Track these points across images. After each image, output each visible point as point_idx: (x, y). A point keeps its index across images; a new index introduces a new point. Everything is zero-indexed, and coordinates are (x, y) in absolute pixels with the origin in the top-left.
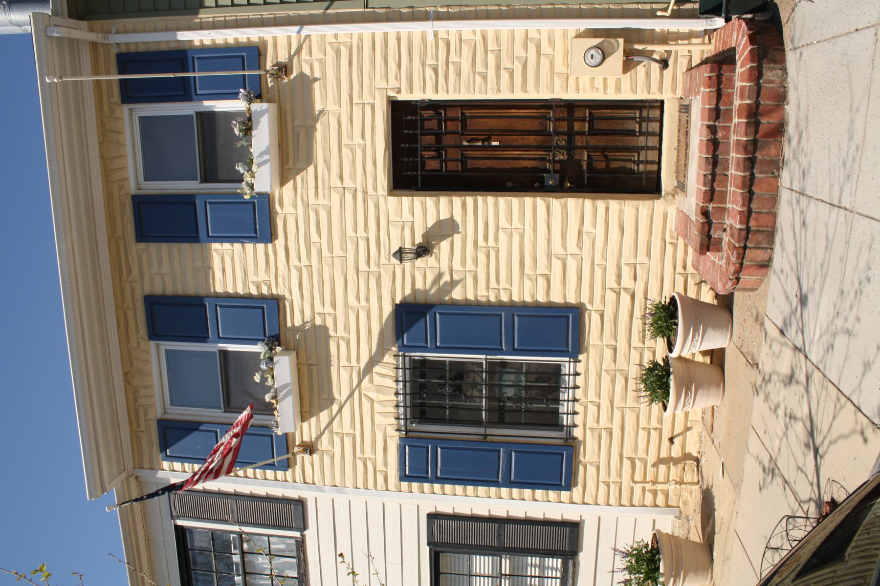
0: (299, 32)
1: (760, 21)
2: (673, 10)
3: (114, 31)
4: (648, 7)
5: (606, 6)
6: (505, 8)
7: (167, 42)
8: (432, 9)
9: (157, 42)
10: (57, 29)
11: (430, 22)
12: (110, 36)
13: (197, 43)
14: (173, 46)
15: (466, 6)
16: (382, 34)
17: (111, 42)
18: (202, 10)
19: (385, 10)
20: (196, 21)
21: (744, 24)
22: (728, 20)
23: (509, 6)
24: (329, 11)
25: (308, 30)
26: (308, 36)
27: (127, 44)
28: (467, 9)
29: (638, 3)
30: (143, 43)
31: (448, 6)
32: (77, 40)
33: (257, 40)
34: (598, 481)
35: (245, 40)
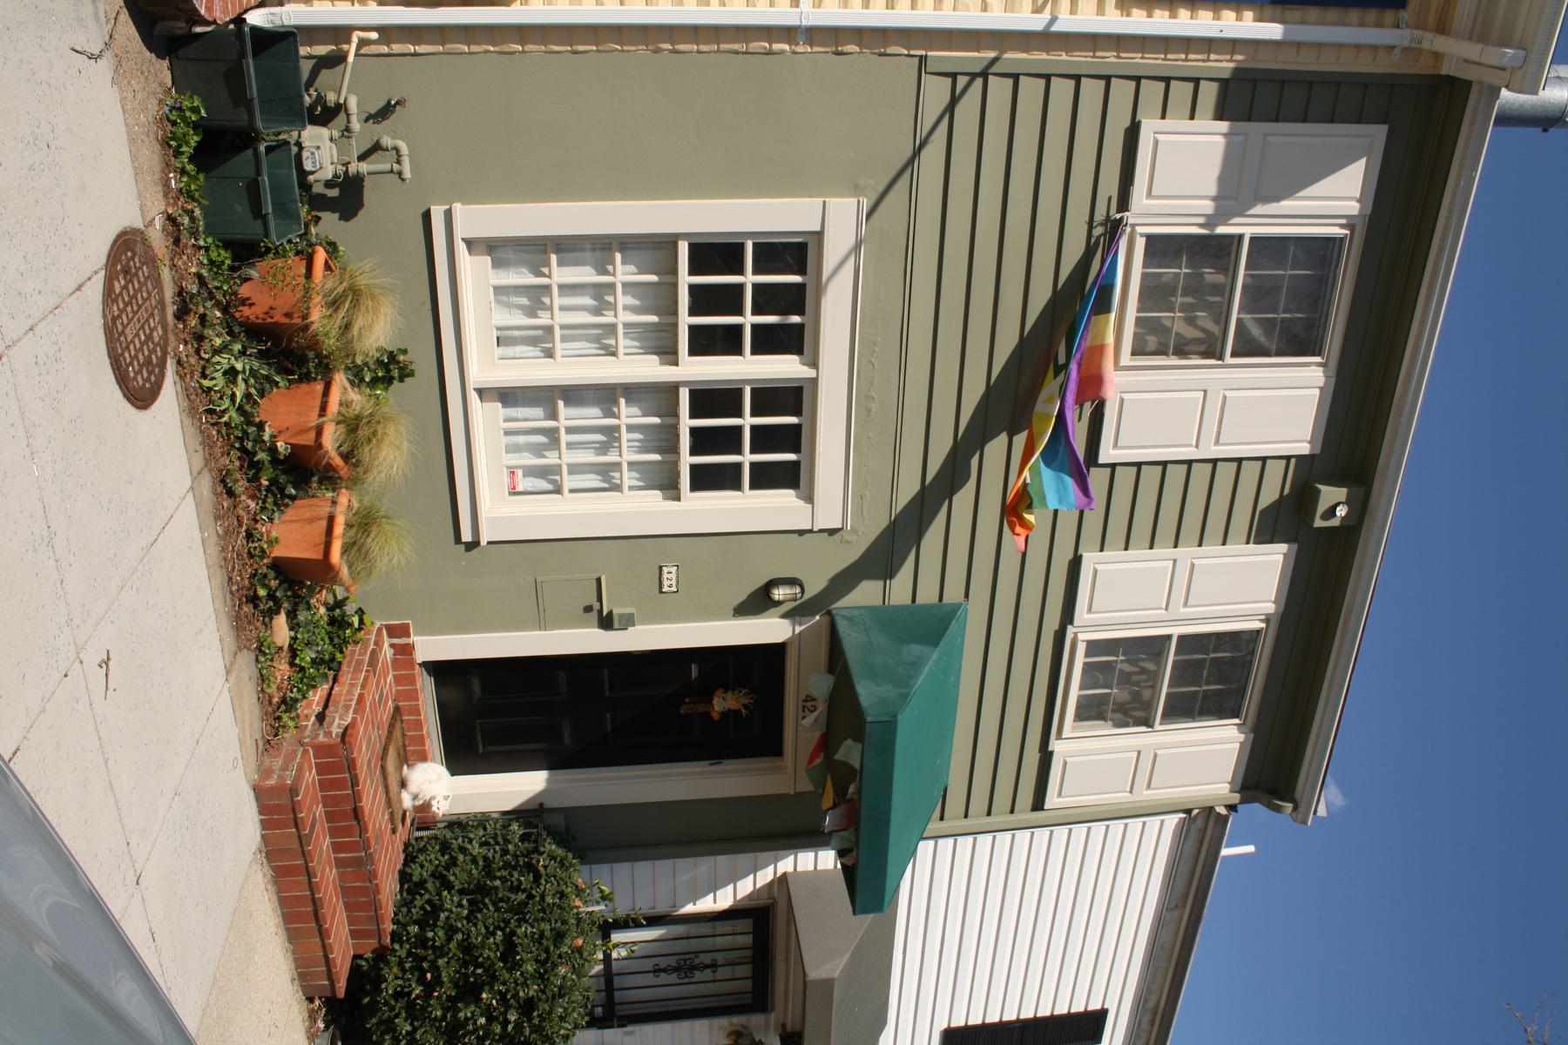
0: (1054, 19)
1: (175, 18)
2: (349, 42)
3: (1397, 51)
4: (397, 48)
5: (474, 48)
6: (664, 46)
7: (1303, 22)
8: (800, 49)
9: (1323, 23)
10: (1503, 63)
11: (805, 23)
12: (1406, 43)
13: (1249, 15)
14: (1295, 13)
15: (737, 53)
16: (898, 6)
17: (1408, 31)
18: (1226, 75)
19: (889, 51)
20: (1240, 57)
21: (203, 12)
22: (239, 21)
23: (657, 51)
24: (992, 54)
25: (1037, 23)
26: (1038, 10)
27: (1379, 25)
28: (736, 47)
29: (415, 54)
30: (1349, 25)
31: (770, 53)
32: (1470, 39)
33: (1135, 11)
34: (746, 53)
35: (1157, 12)
